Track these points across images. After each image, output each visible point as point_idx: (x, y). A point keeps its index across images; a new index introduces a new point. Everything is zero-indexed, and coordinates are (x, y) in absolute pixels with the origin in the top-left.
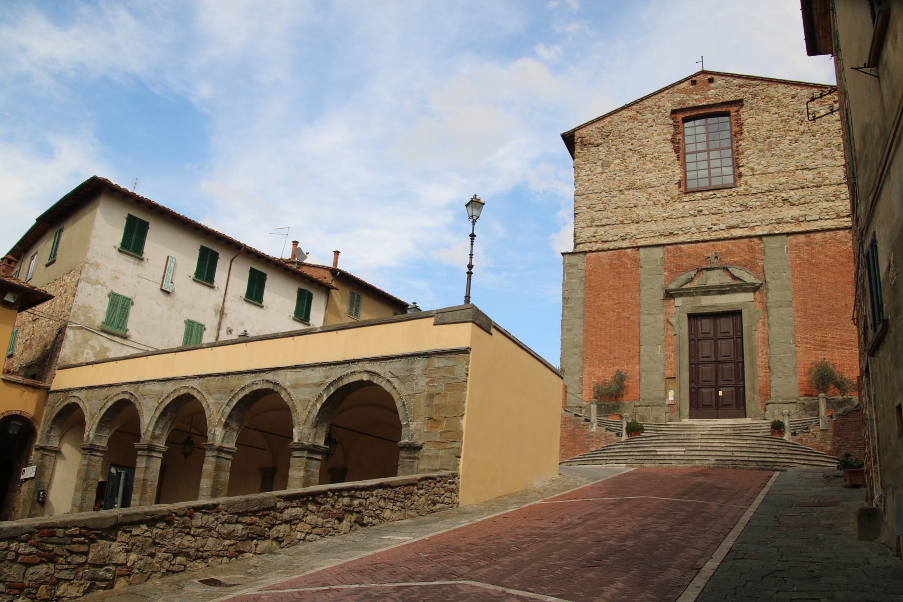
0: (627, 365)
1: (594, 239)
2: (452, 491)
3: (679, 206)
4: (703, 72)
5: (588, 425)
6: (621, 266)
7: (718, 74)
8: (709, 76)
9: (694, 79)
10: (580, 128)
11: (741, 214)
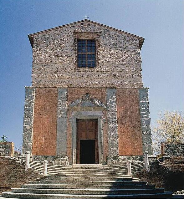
2: (43, 163)
3: (75, 73)
4: (86, 20)
7: (92, 22)
8: (89, 23)
9: (83, 23)
10: (36, 34)
11: (98, 79)
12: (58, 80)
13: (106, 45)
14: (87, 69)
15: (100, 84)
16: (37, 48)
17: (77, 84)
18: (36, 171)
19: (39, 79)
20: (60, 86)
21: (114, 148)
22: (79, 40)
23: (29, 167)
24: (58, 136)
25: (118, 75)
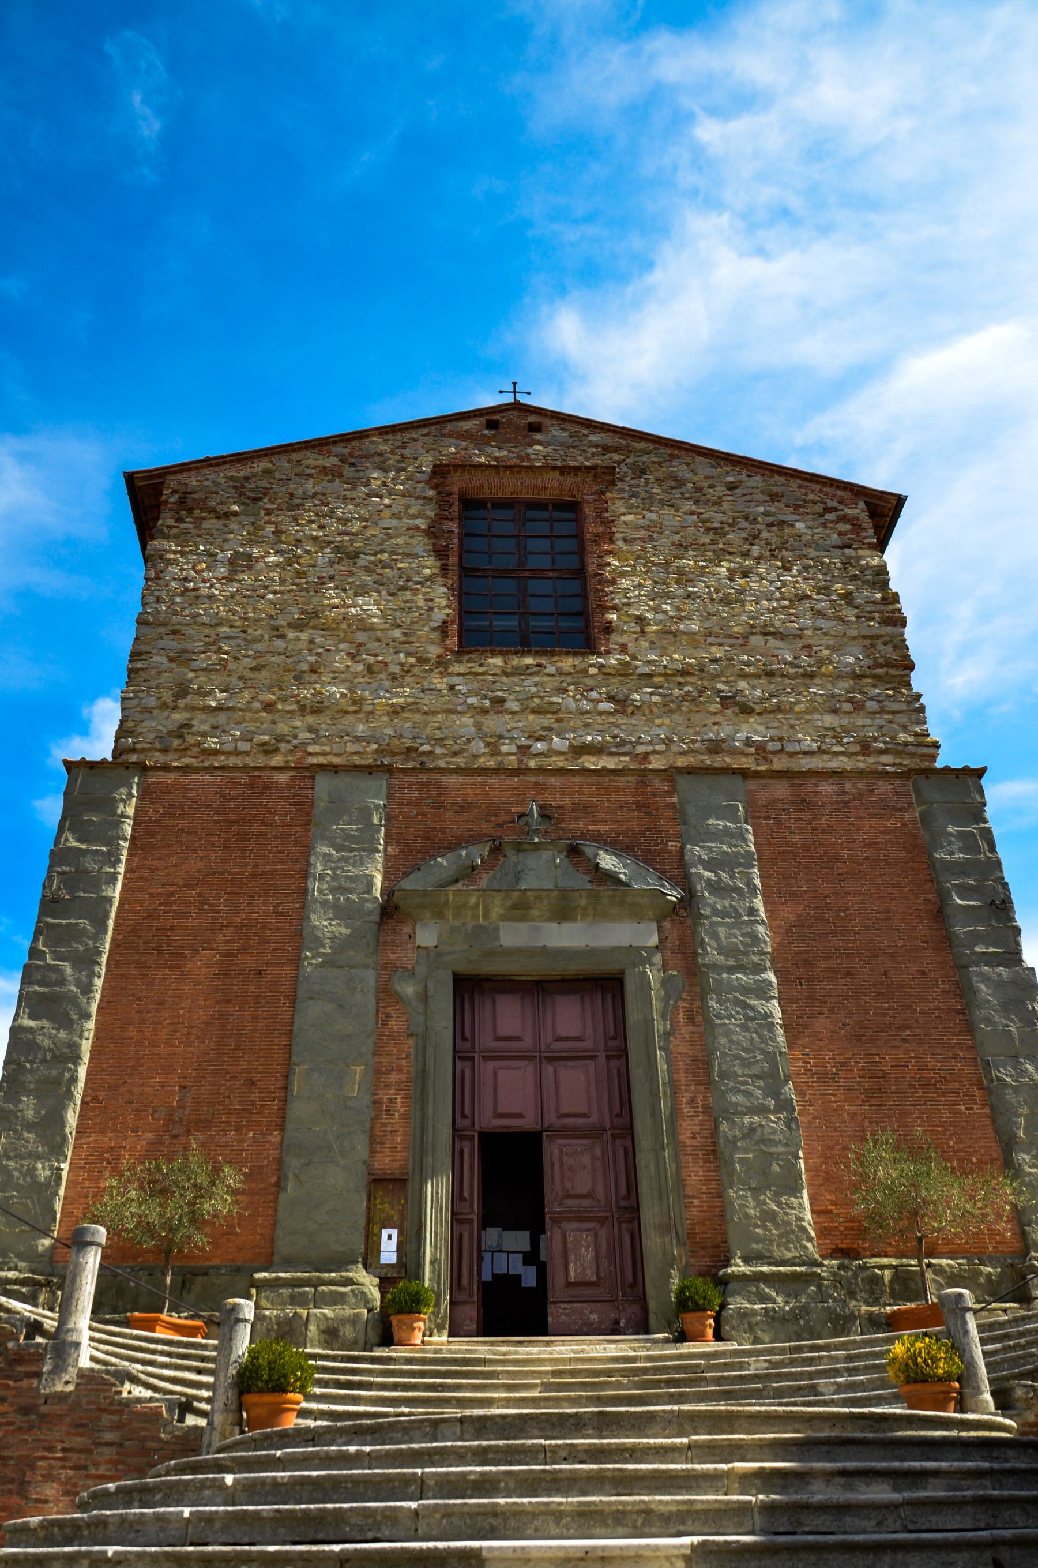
0: (238, 1129)
1: (176, 743)
3: (440, 683)
4: (517, 407)
8: (532, 419)
12: (322, 721)
13: (653, 530)
14: (529, 661)
15: (622, 750)
16: (182, 539)
17: (456, 748)
18: (139, 1392)
19: (178, 717)
20: (336, 760)
21: (767, 1197)
22: (470, 504)
23: (85, 1363)
24: (299, 1110)
25: (751, 691)
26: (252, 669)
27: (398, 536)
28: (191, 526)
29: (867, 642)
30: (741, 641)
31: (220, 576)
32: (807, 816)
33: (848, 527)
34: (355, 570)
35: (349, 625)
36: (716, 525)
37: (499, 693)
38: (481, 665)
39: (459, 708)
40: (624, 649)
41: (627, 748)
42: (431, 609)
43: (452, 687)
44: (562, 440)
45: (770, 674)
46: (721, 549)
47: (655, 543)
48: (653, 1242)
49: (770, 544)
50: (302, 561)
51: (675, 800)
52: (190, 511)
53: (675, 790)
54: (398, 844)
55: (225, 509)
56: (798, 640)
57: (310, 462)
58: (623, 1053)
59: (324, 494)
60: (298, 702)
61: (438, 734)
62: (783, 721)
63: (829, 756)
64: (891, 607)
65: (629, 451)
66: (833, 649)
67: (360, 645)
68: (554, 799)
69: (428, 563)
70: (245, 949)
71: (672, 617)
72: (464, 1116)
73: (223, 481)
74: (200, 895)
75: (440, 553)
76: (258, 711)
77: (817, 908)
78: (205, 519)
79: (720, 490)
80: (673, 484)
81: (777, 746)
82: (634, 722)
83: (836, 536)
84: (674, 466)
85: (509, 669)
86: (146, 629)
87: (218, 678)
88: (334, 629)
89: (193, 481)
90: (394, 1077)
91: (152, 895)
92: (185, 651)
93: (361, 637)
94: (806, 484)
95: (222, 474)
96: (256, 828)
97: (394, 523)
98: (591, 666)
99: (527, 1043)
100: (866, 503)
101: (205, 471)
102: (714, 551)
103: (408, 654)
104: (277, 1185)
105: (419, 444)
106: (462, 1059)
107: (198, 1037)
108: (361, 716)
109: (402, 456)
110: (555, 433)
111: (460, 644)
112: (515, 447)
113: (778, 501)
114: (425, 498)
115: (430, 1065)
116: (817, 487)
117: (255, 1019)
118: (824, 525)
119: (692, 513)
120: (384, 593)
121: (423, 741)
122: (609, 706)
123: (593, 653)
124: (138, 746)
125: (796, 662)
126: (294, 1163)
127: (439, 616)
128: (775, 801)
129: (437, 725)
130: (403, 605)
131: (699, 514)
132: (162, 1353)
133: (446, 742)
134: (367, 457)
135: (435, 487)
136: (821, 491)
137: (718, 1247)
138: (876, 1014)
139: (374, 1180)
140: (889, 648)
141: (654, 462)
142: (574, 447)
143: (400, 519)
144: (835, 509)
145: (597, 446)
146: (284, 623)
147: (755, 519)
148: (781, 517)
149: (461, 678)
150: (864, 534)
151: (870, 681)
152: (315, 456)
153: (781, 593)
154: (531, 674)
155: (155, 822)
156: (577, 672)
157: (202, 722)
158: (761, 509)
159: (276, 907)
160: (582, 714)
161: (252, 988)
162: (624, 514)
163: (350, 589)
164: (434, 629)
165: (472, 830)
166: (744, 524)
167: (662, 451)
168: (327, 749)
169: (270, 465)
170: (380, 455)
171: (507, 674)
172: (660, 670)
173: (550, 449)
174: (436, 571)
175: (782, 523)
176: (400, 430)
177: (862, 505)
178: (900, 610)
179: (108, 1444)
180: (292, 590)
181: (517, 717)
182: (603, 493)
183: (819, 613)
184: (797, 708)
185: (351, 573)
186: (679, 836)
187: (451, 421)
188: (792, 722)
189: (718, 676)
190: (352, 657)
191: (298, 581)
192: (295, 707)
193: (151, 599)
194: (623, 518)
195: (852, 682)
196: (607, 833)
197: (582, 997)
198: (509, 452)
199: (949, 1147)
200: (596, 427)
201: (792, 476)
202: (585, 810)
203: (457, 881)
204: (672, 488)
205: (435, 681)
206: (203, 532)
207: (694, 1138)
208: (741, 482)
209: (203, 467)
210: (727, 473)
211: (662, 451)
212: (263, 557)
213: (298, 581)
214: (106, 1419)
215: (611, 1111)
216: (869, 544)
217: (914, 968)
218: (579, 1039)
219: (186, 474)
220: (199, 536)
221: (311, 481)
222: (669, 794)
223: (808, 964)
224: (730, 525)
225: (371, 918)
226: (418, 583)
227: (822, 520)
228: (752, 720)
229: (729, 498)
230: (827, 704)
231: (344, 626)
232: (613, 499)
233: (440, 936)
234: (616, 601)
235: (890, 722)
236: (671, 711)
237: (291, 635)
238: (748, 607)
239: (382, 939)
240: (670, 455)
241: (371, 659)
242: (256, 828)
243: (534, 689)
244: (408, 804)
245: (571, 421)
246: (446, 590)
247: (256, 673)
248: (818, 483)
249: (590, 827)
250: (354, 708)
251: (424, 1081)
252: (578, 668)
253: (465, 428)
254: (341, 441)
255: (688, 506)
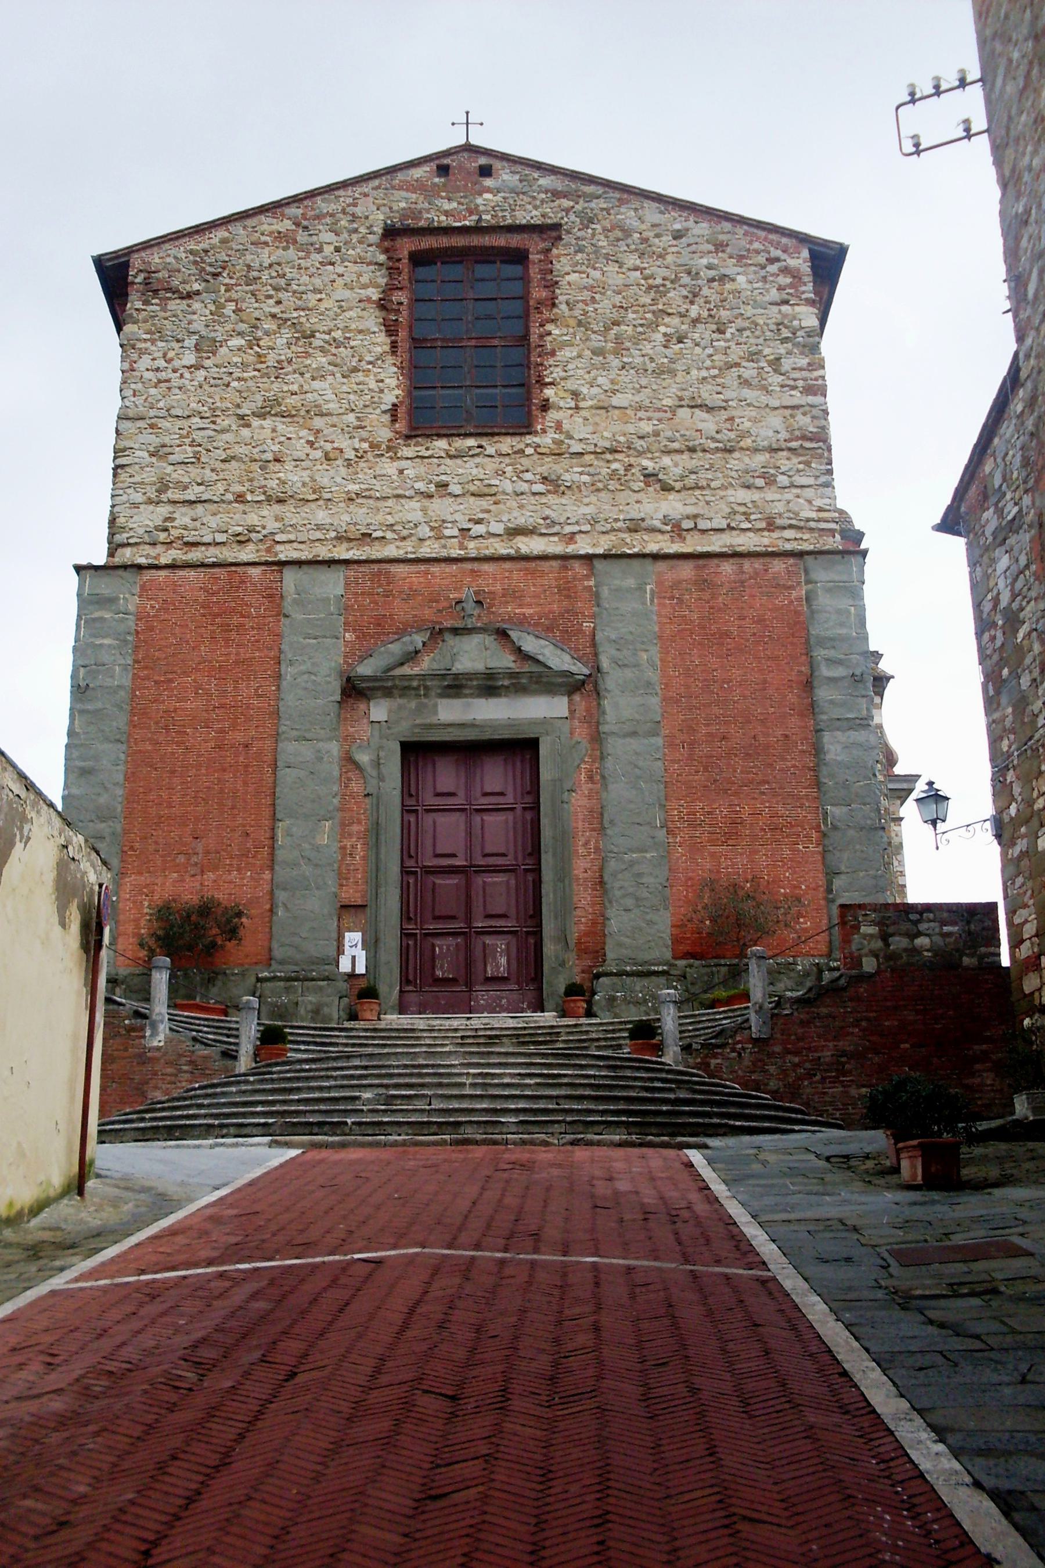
1: (162, 536)
3: (390, 468)
4: (469, 148)
5: (142, 1029)
6: (233, 610)
7: (504, 157)
8: (483, 161)
10: (146, 245)
17: (405, 533)
25: (672, 466)
26: (223, 461)
27: (351, 309)
28: (158, 308)
29: (788, 412)
30: (669, 415)
31: (188, 364)
32: (707, 596)
33: (788, 280)
34: (311, 351)
35: (308, 412)
36: (659, 281)
37: (443, 478)
38: (427, 449)
39: (407, 494)
40: (559, 426)
41: (556, 529)
42: (382, 391)
43: (401, 472)
44: (511, 185)
45: (692, 450)
46: (661, 311)
47: (596, 306)
48: (549, 949)
49: (709, 302)
50: (261, 343)
51: (592, 583)
52: (156, 292)
53: (593, 574)
54: (354, 631)
55: (188, 288)
56: (723, 411)
57: (265, 227)
58: (535, 807)
59: (279, 264)
60: (265, 493)
61: (390, 520)
62: (700, 497)
63: (738, 532)
64: (816, 374)
65: (577, 196)
66: (755, 421)
67: (318, 431)
68: (486, 585)
69: (379, 340)
70: (234, 727)
71: (606, 391)
72: (410, 857)
73: (184, 255)
74: (195, 681)
75: (390, 329)
76: (230, 502)
77: (705, 680)
78: (170, 299)
79: (667, 239)
80: (620, 234)
81: (691, 525)
82: (564, 501)
83: (775, 290)
84: (622, 214)
85: (453, 452)
86: (128, 424)
87: (194, 472)
88: (294, 416)
89: (155, 258)
90: (355, 828)
91: (156, 682)
92: (164, 446)
93: (318, 422)
94: (752, 230)
95: (182, 248)
96: (236, 620)
97: (347, 294)
98: (527, 445)
99: (459, 800)
100: (810, 250)
101: (167, 246)
102: (654, 312)
103: (362, 440)
104: (271, 910)
105: (371, 199)
106: (408, 811)
107: (204, 799)
108: (321, 502)
109: (353, 215)
110: (505, 177)
111: (412, 428)
112: (465, 197)
113: (723, 251)
114: (376, 264)
115: (382, 820)
116: (762, 234)
117: (245, 783)
118: (764, 279)
119: (636, 269)
120: (338, 375)
121: (376, 528)
122: (539, 488)
123: (529, 433)
124: (131, 541)
125: (718, 436)
126: (281, 896)
127: (389, 398)
128: (680, 582)
129: (388, 510)
130: (355, 387)
131: (642, 270)
132: (205, 1026)
133: (395, 528)
134: (318, 217)
135: (386, 251)
136: (766, 239)
137: (597, 952)
138: (742, 772)
139: (342, 906)
140: (807, 419)
141: (602, 209)
142: (523, 193)
143: (352, 289)
144: (777, 260)
145: (546, 192)
146: (249, 412)
147: (697, 273)
148: (723, 271)
149: (409, 462)
150: (803, 288)
151: (785, 453)
152: (269, 220)
153: (712, 361)
154: (473, 456)
155: (153, 616)
156: (515, 453)
157: (184, 515)
158: (704, 261)
159: (256, 690)
160: (518, 495)
161: (241, 759)
162: (568, 274)
163: (308, 371)
164: (384, 412)
165: (416, 616)
166: (686, 279)
167: (612, 195)
168: (292, 537)
169: (226, 234)
170: (332, 215)
171: (451, 457)
172: (591, 448)
173: (499, 198)
174: (387, 348)
175: (723, 278)
176: (352, 185)
177: (805, 253)
178: (823, 378)
179: (186, 1072)
180: (254, 377)
181: (459, 500)
182: (549, 250)
183: (746, 383)
184: (713, 484)
185: (308, 355)
186: (593, 616)
187: (401, 169)
188: (708, 498)
189: (644, 452)
190: (311, 444)
191: (259, 366)
192: (263, 498)
193: (130, 393)
194: (567, 278)
195: (768, 455)
196: (531, 616)
197: (505, 760)
198: (459, 203)
199: (785, 877)
200: (545, 169)
201: (738, 222)
202: (513, 595)
203: (402, 664)
204: (618, 240)
205: (386, 466)
206: (169, 314)
207: (586, 872)
208: (687, 230)
209: (163, 242)
210: (675, 219)
211: (612, 195)
212: (226, 341)
213: (259, 366)
214: (184, 1060)
215: (524, 850)
216: (807, 300)
217: (779, 732)
218: (502, 794)
219: (148, 252)
220: (166, 319)
221: (267, 250)
222: (587, 577)
223: (692, 730)
224: (672, 282)
225: (332, 698)
226: (370, 363)
227: (763, 273)
228: (671, 497)
229: (674, 249)
230: (742, 480)
231: (302, 413)
232: (558, 256)
233: (390, 711)
234: (555, 375)
235: (798, 497)
236: (598, 490)
237: (256, 422)
238: (678, 379)
239: (342, 716)
240: (619, 200)
241: (328, 447)
242: (236, 620)
243: (475, 471)
244: (363, 594)
245: (521, 163)
246: (396, 369)
247: (227, 464)
248: (764, 229)
249: (517, 611)
250: (315, 496)
251: (377, 834)
252: (515, 449)
253: (415, 176)
254: (294, 202)
255: (633, 260)
